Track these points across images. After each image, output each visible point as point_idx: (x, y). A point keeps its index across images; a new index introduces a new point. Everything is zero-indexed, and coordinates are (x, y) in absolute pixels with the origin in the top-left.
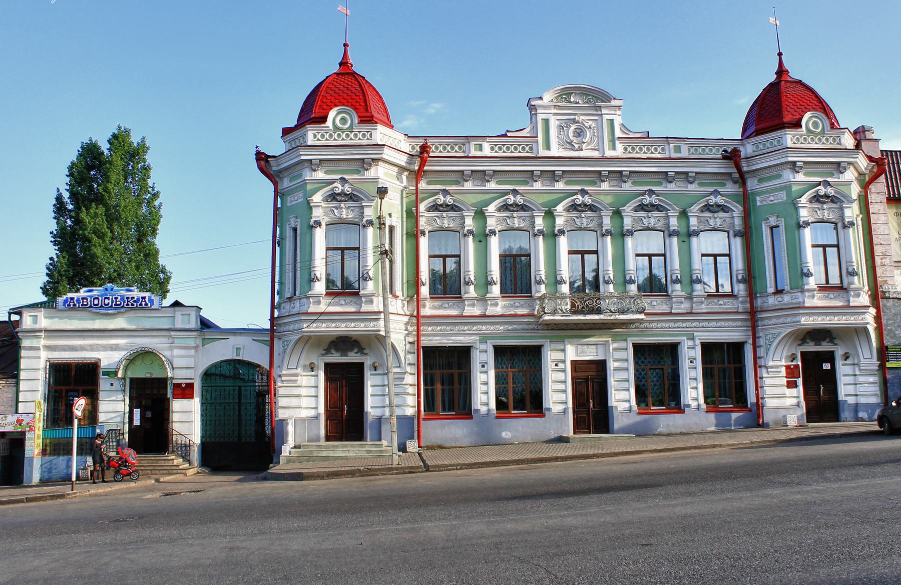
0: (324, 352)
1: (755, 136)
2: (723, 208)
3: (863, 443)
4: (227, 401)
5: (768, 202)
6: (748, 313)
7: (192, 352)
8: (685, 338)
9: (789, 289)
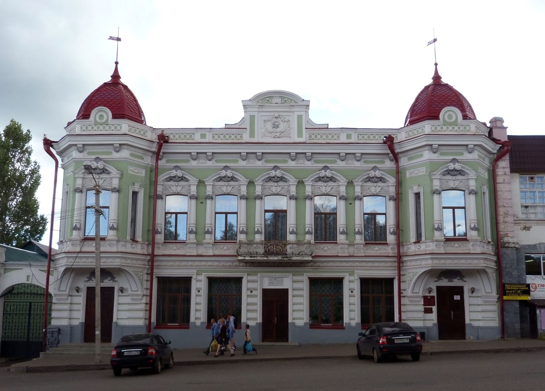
0: (87, 279)
1: (82, 119)
2: (381, 179)
3: (283, 343)
4: (21, 313)
5: (414, 175)
8: (348, 274)
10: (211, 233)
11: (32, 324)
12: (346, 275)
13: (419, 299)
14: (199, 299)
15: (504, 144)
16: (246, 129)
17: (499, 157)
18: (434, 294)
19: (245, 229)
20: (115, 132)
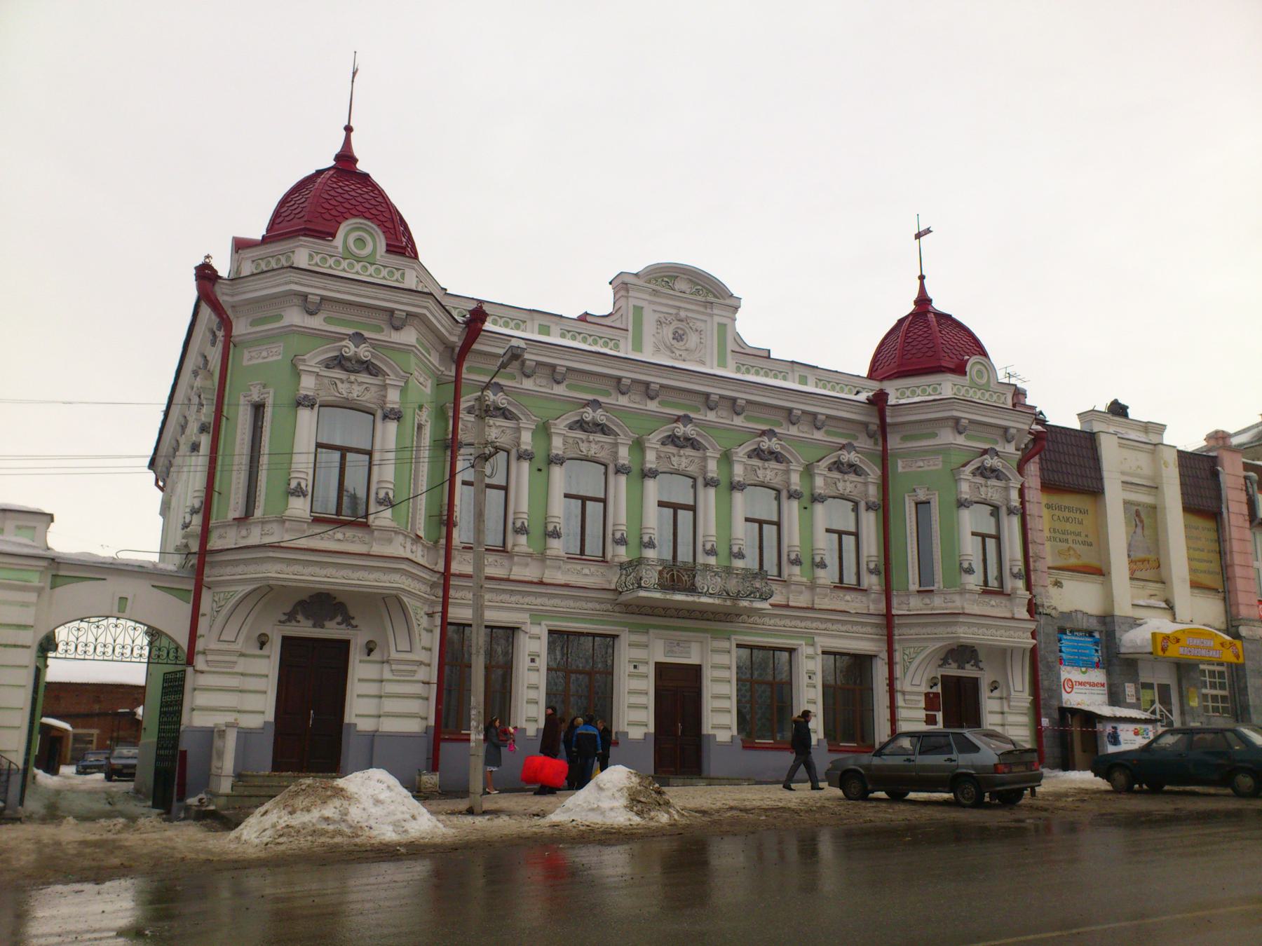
0: (284, 618)
2: (854, 468)
6: (883, 615)
7: (32, 597)
9: (942, 587)
12: (800, 645)
18: (938, 689)
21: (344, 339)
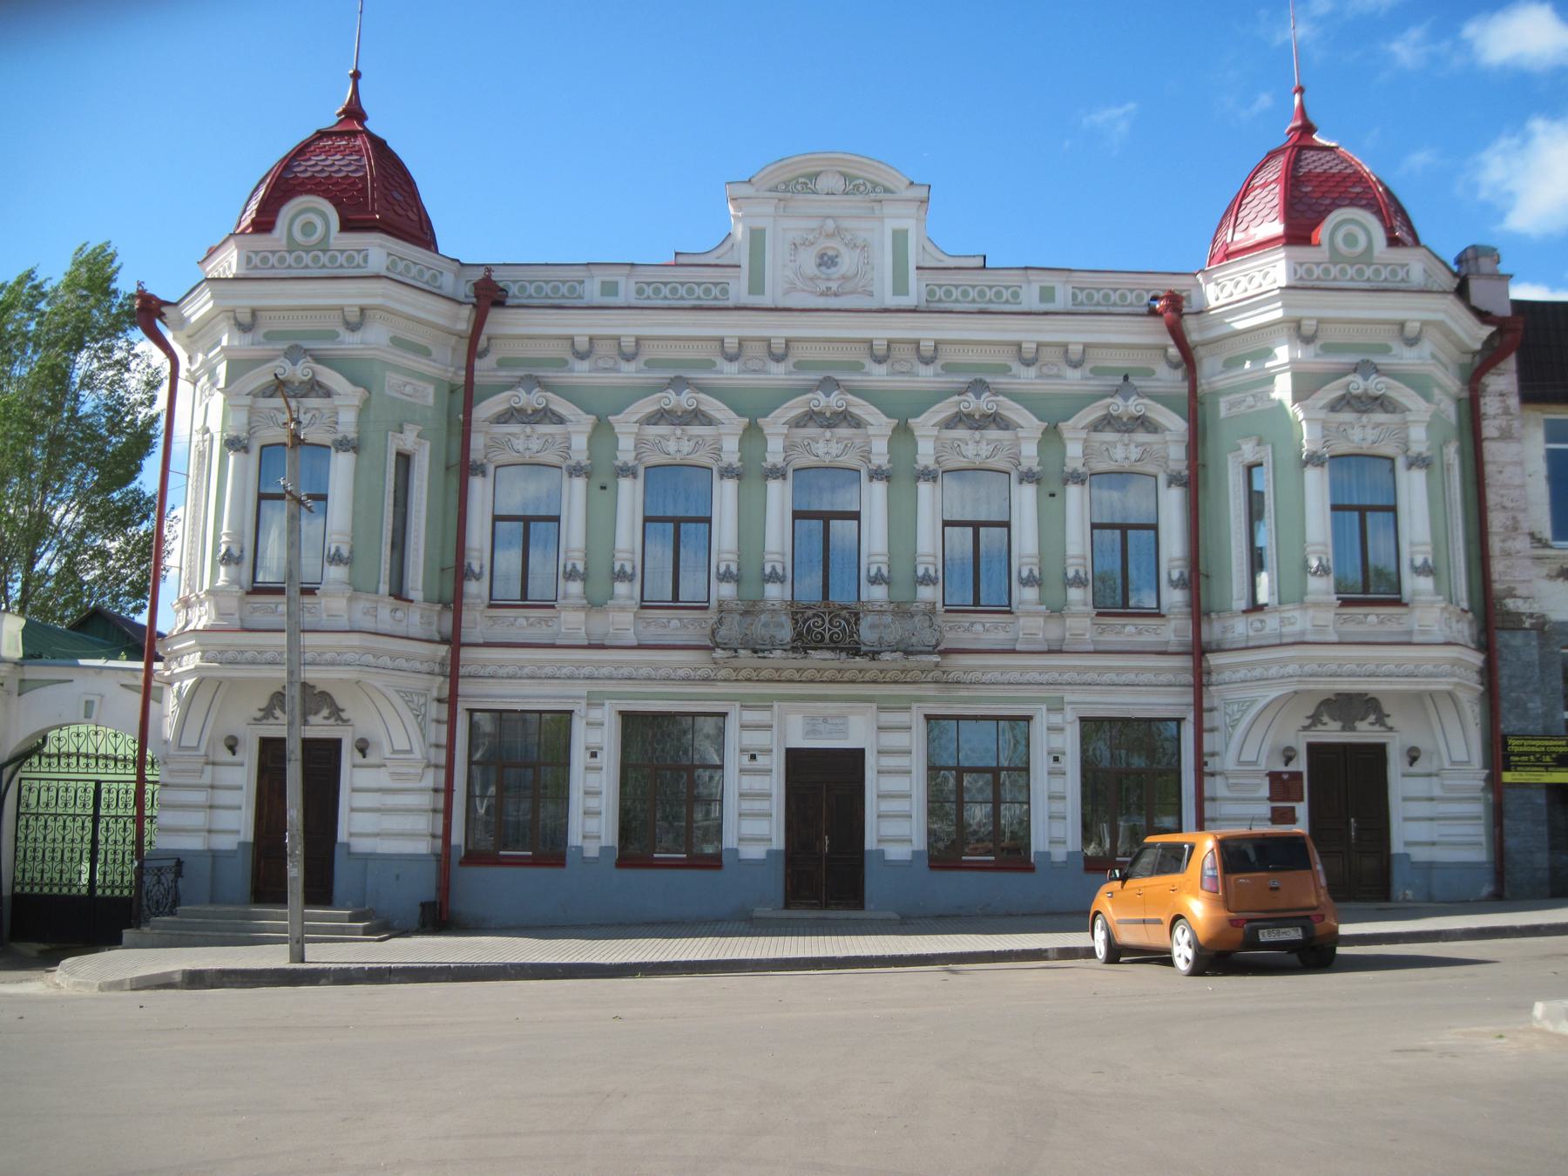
2: (1143, 423)
4: (71, 811)
5: (1243, 408)
8: (1044, 707)
10: (631, 578)
11: (101, 847)
13: (1258, 781)
14: (593, 780)
15: (1501, 325)
16: (739, 266)
17: (1488, 359)
18: (1301, 765)
19: (734, 568)
20: (313, 271)
21: (279, 356)
